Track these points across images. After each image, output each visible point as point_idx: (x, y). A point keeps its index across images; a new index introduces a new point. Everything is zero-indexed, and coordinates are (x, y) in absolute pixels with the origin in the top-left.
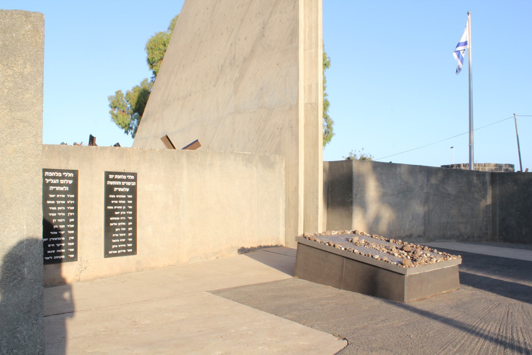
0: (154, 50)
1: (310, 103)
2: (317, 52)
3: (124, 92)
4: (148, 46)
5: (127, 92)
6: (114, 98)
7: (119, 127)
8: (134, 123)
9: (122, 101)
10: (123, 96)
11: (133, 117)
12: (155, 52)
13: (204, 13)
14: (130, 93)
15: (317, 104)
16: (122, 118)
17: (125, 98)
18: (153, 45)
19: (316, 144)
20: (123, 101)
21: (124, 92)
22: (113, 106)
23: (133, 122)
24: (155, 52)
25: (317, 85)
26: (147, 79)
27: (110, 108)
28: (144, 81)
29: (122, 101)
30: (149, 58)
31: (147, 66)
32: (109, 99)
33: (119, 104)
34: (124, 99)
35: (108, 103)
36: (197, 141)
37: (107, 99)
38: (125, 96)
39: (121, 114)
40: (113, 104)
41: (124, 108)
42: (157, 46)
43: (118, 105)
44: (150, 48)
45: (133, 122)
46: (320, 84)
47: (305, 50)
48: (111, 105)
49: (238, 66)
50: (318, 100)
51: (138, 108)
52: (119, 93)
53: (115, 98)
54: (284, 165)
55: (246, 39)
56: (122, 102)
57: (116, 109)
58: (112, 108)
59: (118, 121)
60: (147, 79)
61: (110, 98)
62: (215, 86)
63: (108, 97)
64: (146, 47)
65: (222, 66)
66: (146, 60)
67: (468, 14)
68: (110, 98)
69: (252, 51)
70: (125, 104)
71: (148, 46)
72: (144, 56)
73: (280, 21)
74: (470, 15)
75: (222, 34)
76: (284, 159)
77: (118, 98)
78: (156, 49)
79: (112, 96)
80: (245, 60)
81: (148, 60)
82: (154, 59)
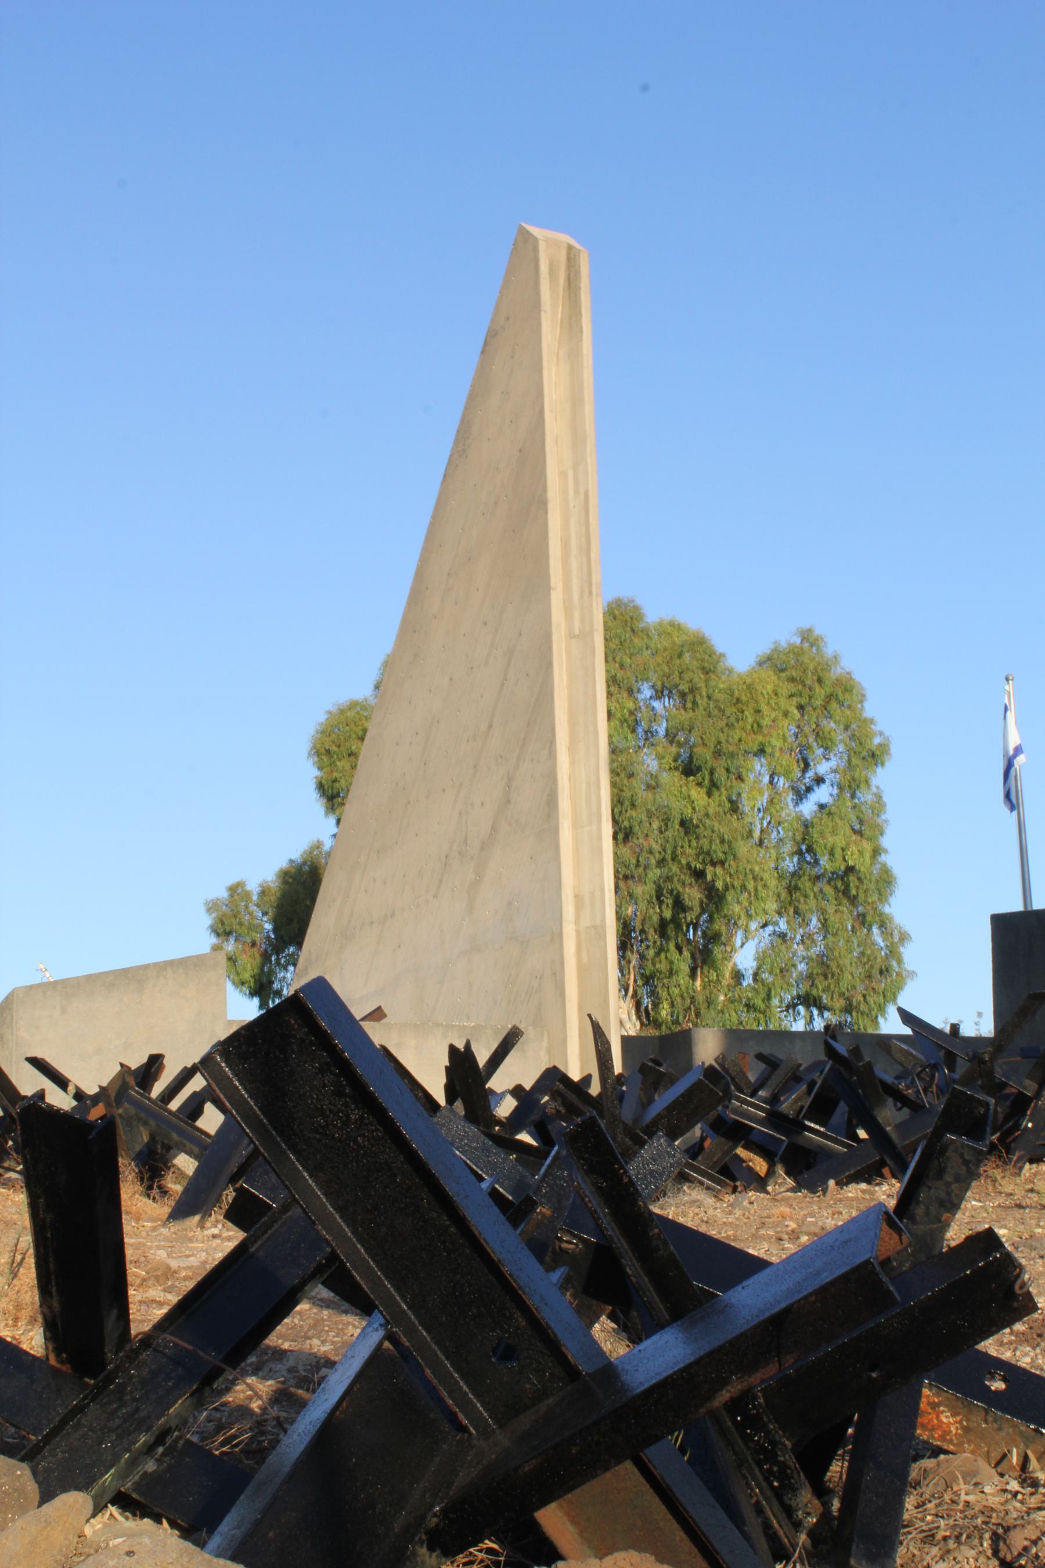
0: (335, 756)
1: (593, 926)
2: (599, 829)
3: (253, 886)
4: (318, 746)
5: (261, 886)
6: (224, 907)
7: (241, 991)
8: (284, 978)
9: (249, 913)
10: (250, 899)
11: (283, 961)
12: (338, 763)
13: (411, 743)
14: (269, 888)
15: (603, 927)
16: (249, 965)
17: (258, 906)
18: (333, 742)
19: (605, 1001)
20: (251, 914)
21: (253, 886)
22: (220, 931)
23: (282, 974)
24: (338, 763)
25: (603, 890)
26: (318, 841)
27: (212, 935)
28: (311, 847)
29: (249, 913)
30: (324, 782)
31: (316, 805)
32: (209, 910)
33: (241, 924)
34: (253, 908)
35: (207, 921)
36: (379, 1008)
37: (203, 909)
38: (255, 898)
39: (245, 953)
40: (223, 923)
41: (254, 934)
42: (344, 746)
43: (238, 927)
44: (323, 751)
45: (282, 974)
46: (609, 890)
47: (576, 826)
48: (215, 928)
49: (472, 858)
50: (605, 919)
51: (297, 931)
52: (239, 891)
53: (227, 905)
54: (545, 1044)
55: (482, 804)
56: (247, 917)
57: (232, 940)
58: (218, 935)
59: (238, 974)
60: (318, 841)
61: (212, 906)
62: (435, 896)
63: (207, 903)
64: (312, 749)
65: (446, 857)
66: (314, 786)
67: (1007, 680)
68: (212, 906)
69: (494, 828)
70: (256, 922)
71: (318, 746)
72: (309, 773)
73: (532, 776)
74: (1010, 682)
75: (444, 791)
76: (546, 1033)
77: (237, 906)
78: (342, 754)
79: (218, 899)
80: (482, 848)
81: (321, 787)
82: (337, 785)
